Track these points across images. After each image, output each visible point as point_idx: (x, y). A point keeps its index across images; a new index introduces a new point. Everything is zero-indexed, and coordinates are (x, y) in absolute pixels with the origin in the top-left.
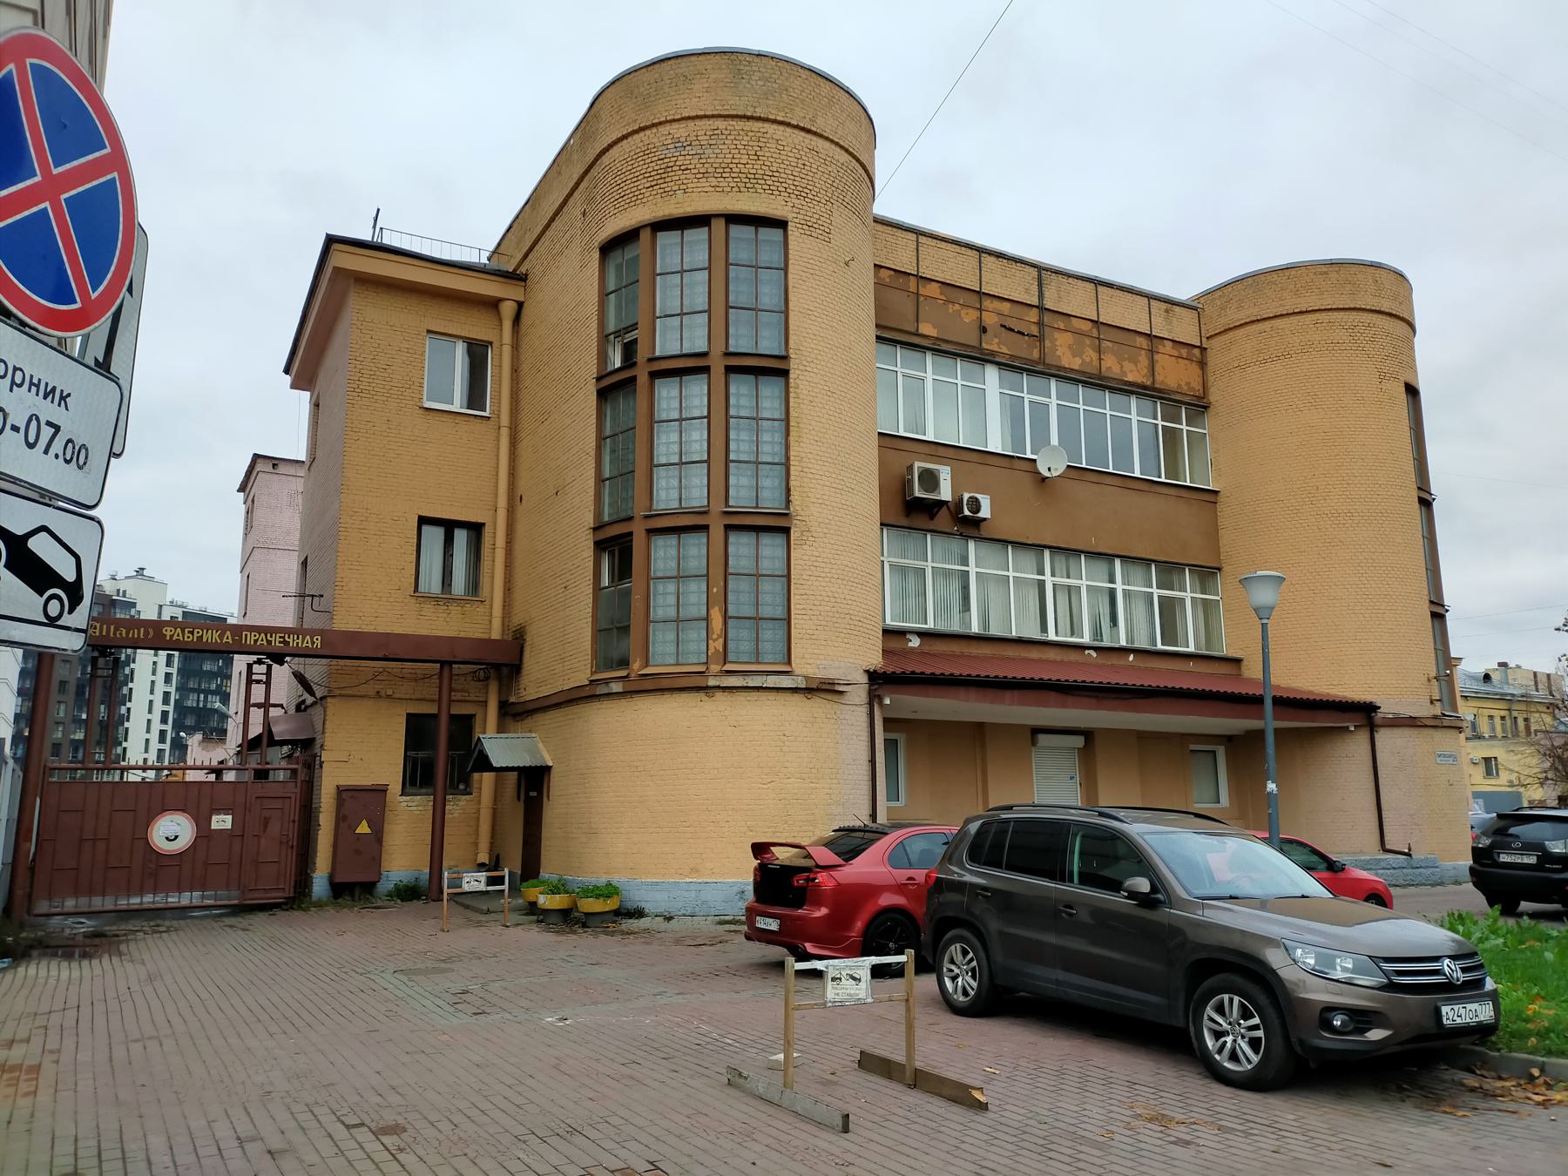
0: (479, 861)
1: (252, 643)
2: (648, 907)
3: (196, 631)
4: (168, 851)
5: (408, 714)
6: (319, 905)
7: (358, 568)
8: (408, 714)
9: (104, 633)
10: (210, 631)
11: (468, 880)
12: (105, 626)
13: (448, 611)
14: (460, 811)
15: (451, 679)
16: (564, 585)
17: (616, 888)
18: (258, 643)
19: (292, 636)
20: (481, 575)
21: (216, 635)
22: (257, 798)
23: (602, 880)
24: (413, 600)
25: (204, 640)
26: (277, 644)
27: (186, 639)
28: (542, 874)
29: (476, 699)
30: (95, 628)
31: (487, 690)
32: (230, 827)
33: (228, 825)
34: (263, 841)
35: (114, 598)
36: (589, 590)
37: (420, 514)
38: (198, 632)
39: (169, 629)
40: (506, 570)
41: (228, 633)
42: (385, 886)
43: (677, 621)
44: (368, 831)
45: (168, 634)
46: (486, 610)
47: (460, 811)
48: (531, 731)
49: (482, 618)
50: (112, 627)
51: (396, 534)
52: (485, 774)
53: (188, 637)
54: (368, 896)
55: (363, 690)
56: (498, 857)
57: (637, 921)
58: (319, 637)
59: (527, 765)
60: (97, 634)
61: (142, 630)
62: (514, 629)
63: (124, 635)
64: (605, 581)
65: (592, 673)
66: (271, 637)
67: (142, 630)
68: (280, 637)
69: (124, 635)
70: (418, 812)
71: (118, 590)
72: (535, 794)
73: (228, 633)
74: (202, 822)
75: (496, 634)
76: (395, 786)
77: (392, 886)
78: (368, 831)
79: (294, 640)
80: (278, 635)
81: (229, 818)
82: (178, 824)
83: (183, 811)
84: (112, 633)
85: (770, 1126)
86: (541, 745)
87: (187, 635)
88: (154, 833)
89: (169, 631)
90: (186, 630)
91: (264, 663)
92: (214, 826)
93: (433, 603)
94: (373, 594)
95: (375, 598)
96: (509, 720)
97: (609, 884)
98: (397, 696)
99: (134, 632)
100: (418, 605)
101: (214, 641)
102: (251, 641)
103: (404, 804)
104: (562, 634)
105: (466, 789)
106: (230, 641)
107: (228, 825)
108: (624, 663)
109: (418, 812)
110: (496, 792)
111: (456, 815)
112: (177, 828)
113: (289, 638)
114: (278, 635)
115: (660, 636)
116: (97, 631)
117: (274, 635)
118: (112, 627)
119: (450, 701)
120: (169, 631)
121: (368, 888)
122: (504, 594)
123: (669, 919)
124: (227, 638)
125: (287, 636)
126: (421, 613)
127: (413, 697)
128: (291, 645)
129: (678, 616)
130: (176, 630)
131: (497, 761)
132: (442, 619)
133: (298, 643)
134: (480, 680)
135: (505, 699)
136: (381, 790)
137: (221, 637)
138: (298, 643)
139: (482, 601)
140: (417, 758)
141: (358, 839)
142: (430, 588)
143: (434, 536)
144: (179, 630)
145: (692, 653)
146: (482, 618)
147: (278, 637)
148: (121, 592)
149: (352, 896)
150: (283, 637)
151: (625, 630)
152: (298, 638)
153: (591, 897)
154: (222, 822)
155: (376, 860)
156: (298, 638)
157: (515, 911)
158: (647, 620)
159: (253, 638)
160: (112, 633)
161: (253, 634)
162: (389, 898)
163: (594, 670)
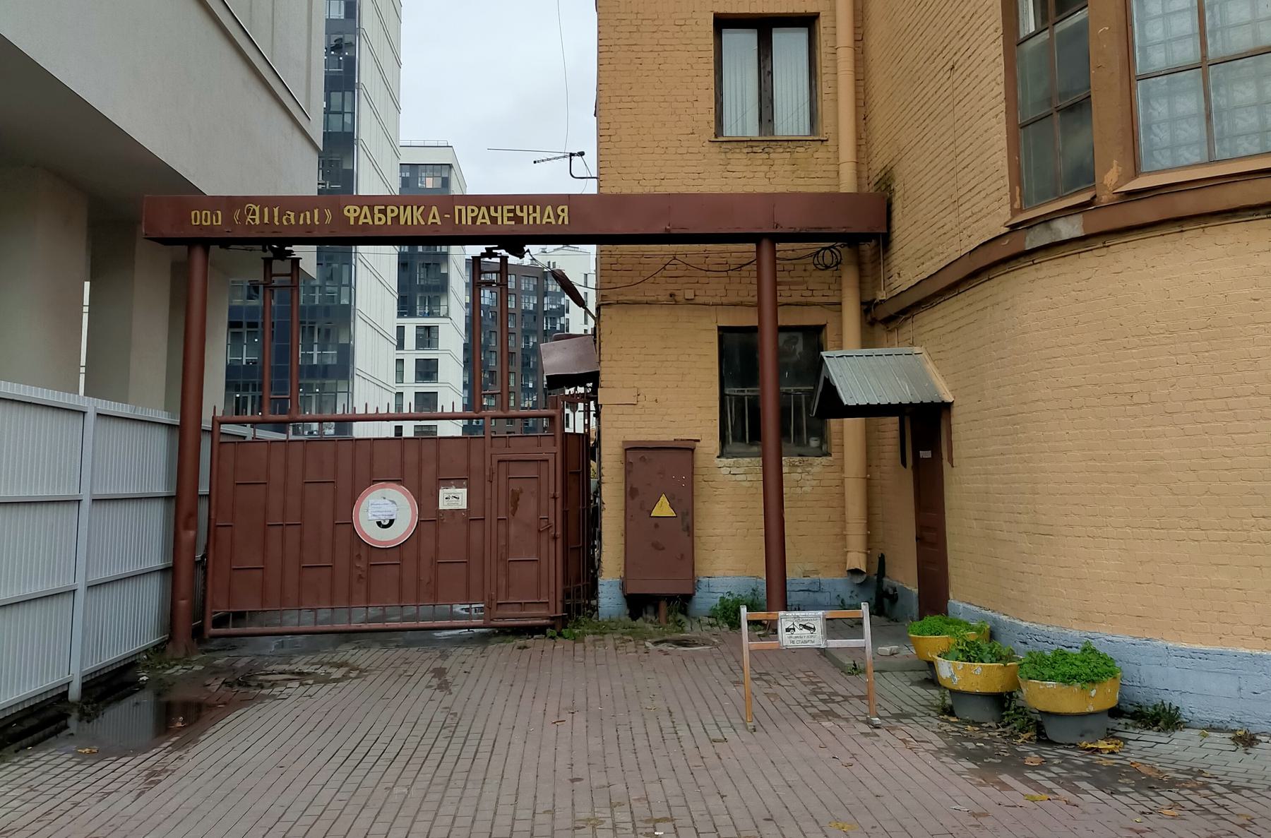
0: (850, 566)
1: (470, 223)
2: (1189, 706)
3: (389, 209)
4: (381, 543)
5: (720, 328)
6: (602, 630)
7: (629, 105)
8: (720, 328)
9: (266, 221)
10: (409, 208)
11: (789, 625)
12: (266, 210)
13: (770, 162)
14: (814, 483)
15: (775, 264)
16: (950, 64)
17: (1108, 661)
18: (478, 223)
19: (525, 207)
20: (819, 99)
21: (417, 214)
22: (499, 461)
23: (1075, 633)
24: (714, 149)
25: (402, 222)
26: (506, 222)
27: (377, 222)
28: (952, 602)
29: (825, 300)
30: (254, 213)
31: (841, 284)
32: (466, 508)
33: (462, 504)
34: (513, 529)
35: (545, 270)
36: (994, 50)
37: (716, 10)
38: (392, 211)
39: (352, 208)
40: (856, 86)
41: (434, 209)
42: (705, 601)
43: (1203, 65)
44: (670, 513)
45: (352, 216)
46: (830, 155)
47: (814, 483)
48: (912, 344)
49: (824, 168)
50: (276, 210)
51: (683, 48)
52: (846, 420)
53: (380, 219)
54: (680, 616)
55: (650, 292)
56: (882, 560)
57: (1163, 738)
58: (566, 208)
59: (906, 401)
60: (257, 222)
61: (316, 211)
62: (877, 179)
63: (293, 222)
64: (1029, 23)
65: (1014, 212)
66: (496, 211)
67: (316, 211)
68: (509, 211)
69: (293, 222)
70: (747, 484)
71: (549, 263)
72: (926, 454)
73: (434, 209)
74: (425, 499)
75: (847, 184)
76: (709, 443)
77: (718, 601)
78: (670, 513)
79: (529, 214)
80: (506, 208)
81: (463, 492)
82: (393, 502)
83: (399, 482)
84: (276, 219)
85: (1248, 798)
86: (930, 366)
87: (377, 215)
88: (361, 514)
89: (352, 211)
90: (376, 209)
91: (495, 255)
92: (443, 505)
93: (745, 151)
94: (655, 144)
95: (658, 150)
96: (879, 329)
97: (1088, 650)
98: (699, 300)
99: (305, 215)
100: (723, 156)
101: (415, 222)
102: (467, 220)
103: (725, 471)
104: (953, 155)
105: (820, 447)
106: (438, 221)
107: (462, 504)
108: (1084, 175)
109: (747, 484)
110: (867, 453)
111: (806, 489)
112: (392, 508)
113: (522, 211)
114: (506, 208)
115: (1160, 109)
116: (257, 217)
117: (499, 208)
118: (276, 210)
119: (776, 305)
120: (352, 211)
121: (682, 603)
122: (857, 126)
123: (1247, 741)
124: (434, 217)
125: (518, 207)
126: (729, 167)
127: (725, 300)
128: (526, 222)
129: (1204, 57)
130: (361, 208)
131: (850, 395)
132: (763, 174)
133: (535, 218)
134: (827, 267)
135: (869, 299)
136: (686, 449)
137: (425, 215)
138: (535, 218)
139: (822, 141)
140: (743, 397)
141: (656, 526)
142: (737, 133)
143: (742, 44)
144: (366, 209)
145: (1247, 135)
146: (824, 168)
147: (505, 211)
148: (551, 264)
149: (656, 612)
150: (513, 211)
151: (1078, 108)
152: (535, 211)
153: (1051, 678)
154: (453, 498)
155: (687, 558)
156: (535, 211)
157: (903, 671)
158: (1130, 76)
159: (470, 215)
160: (276, 219)
161: (469, 208)
162: (711, 620)
163: (1016, 206)
